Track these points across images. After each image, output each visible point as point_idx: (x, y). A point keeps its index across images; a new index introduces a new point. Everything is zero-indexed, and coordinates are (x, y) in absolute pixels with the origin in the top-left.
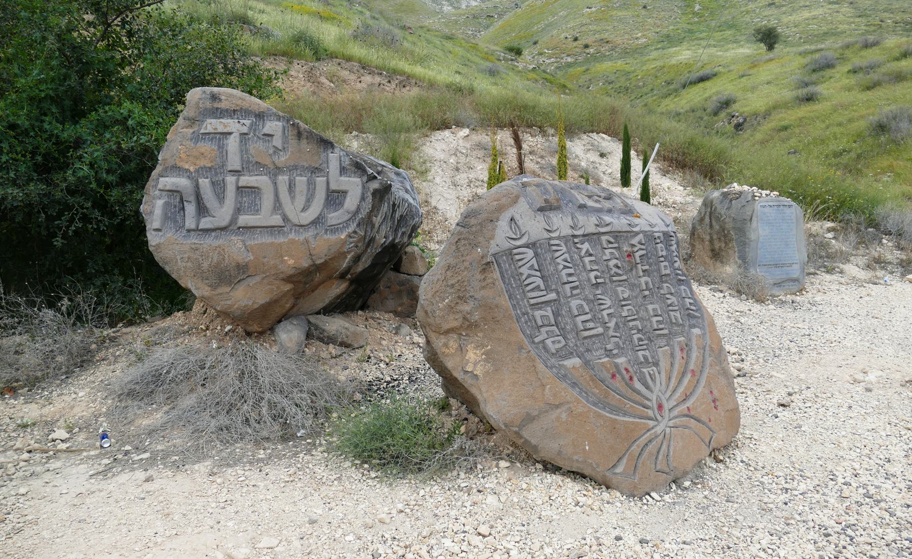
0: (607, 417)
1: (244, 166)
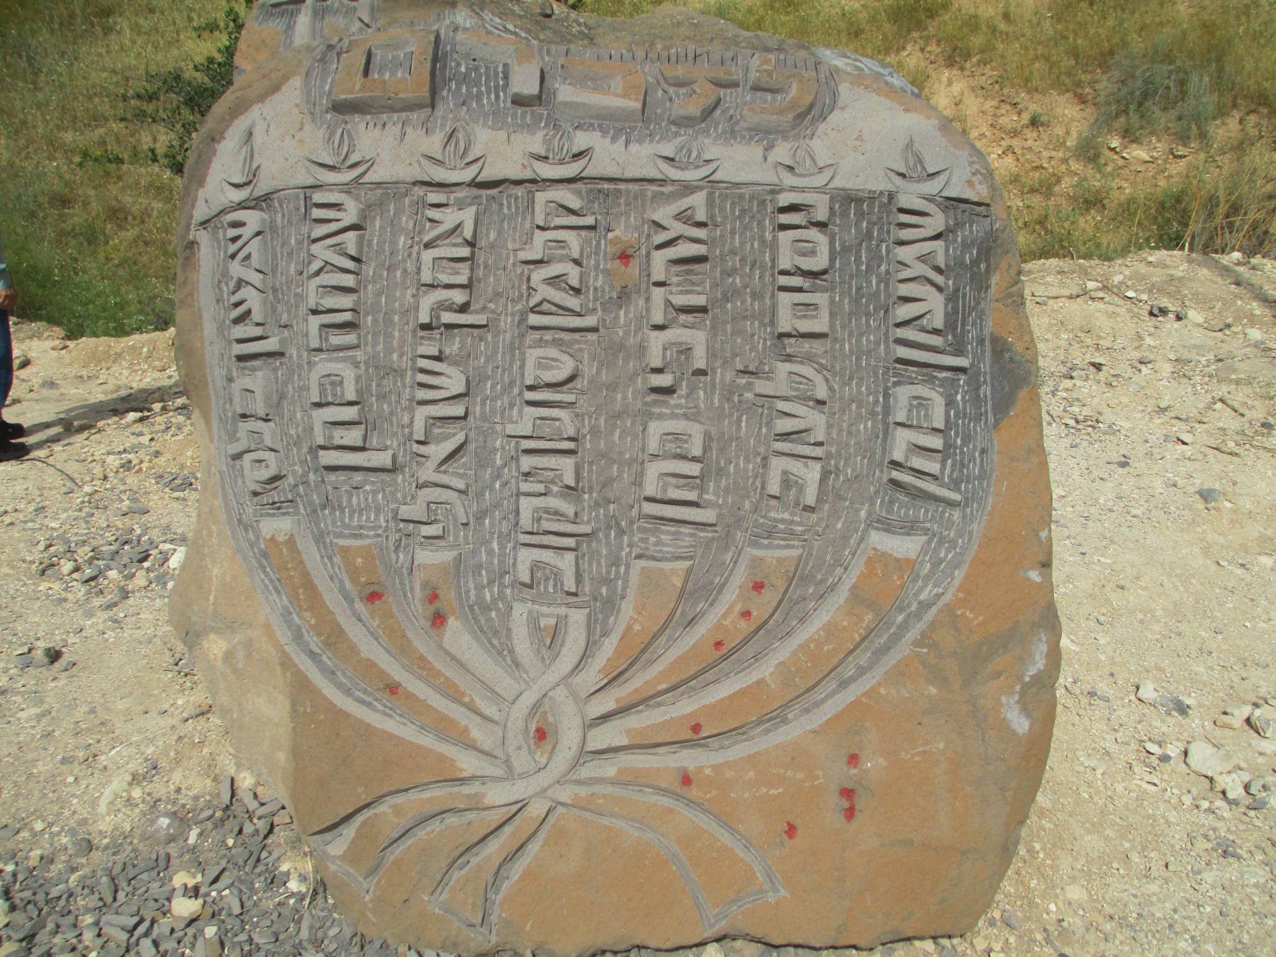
0: (325, 698)
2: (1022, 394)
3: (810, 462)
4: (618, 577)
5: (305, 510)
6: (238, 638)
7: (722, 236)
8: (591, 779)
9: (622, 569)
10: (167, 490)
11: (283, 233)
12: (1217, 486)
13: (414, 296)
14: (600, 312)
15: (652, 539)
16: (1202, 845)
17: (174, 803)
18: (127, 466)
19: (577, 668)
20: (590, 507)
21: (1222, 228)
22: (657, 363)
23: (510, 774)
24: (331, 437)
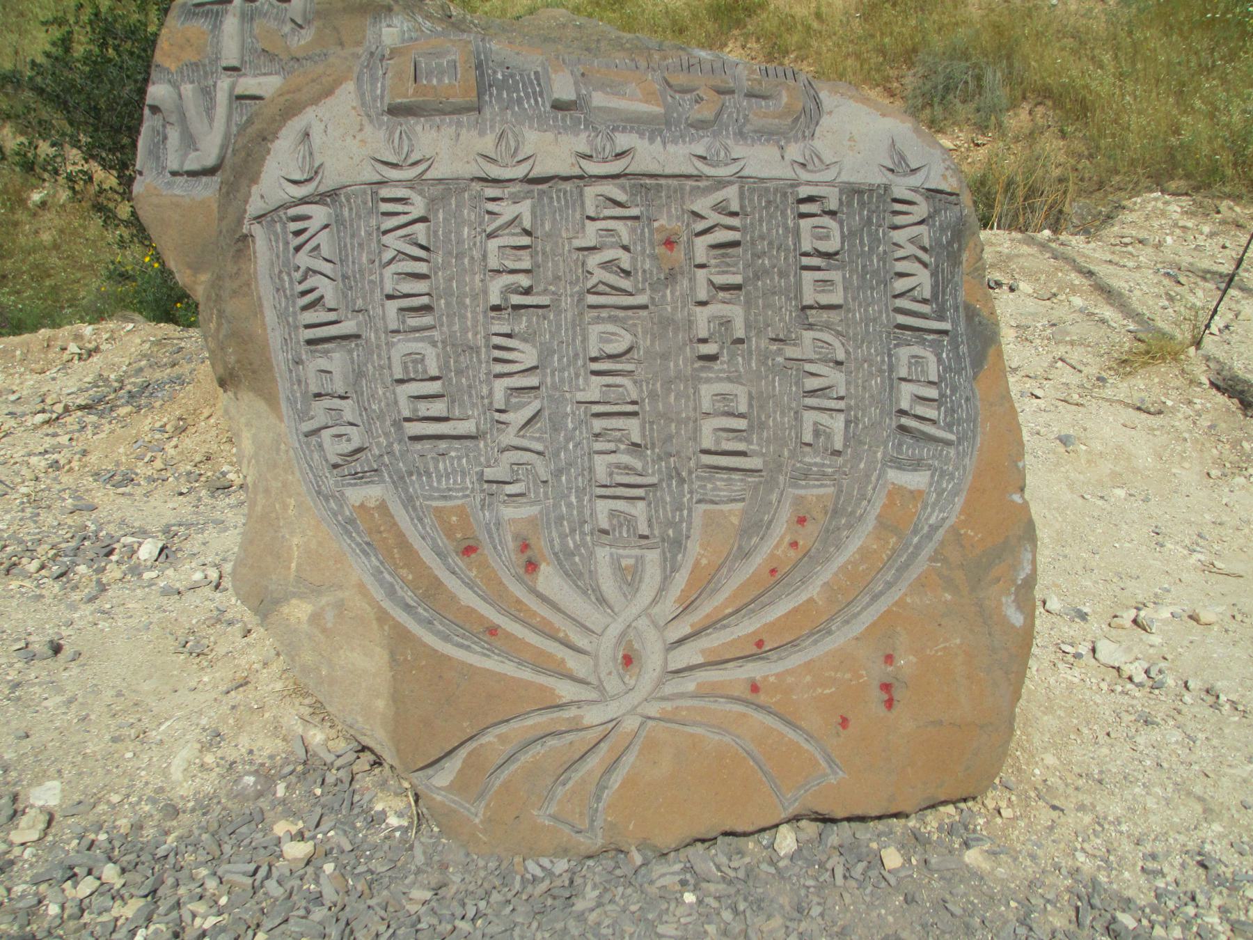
0: (425, 645)
1: (247, 58)
2: (992, 351)
3: (834, 414)
4: (681, 521)
5: (391, 477)
6: (324, 600)
7: (752, 224)
8: (674, 695)
9: (685, 512)
10: (108, 486)
11: (352, 226)
12: (1071, 432)
13: (482, 281)
14: (648, 292)
15: (709, 486)
16: (1127, 718)
17: (251, 763)
18: (55, 465)
19: (654, 601)
20: (653, 461)
21: (1024, 209)
22: (703, 334)
23: (604, 697)
24: (416, 410)
